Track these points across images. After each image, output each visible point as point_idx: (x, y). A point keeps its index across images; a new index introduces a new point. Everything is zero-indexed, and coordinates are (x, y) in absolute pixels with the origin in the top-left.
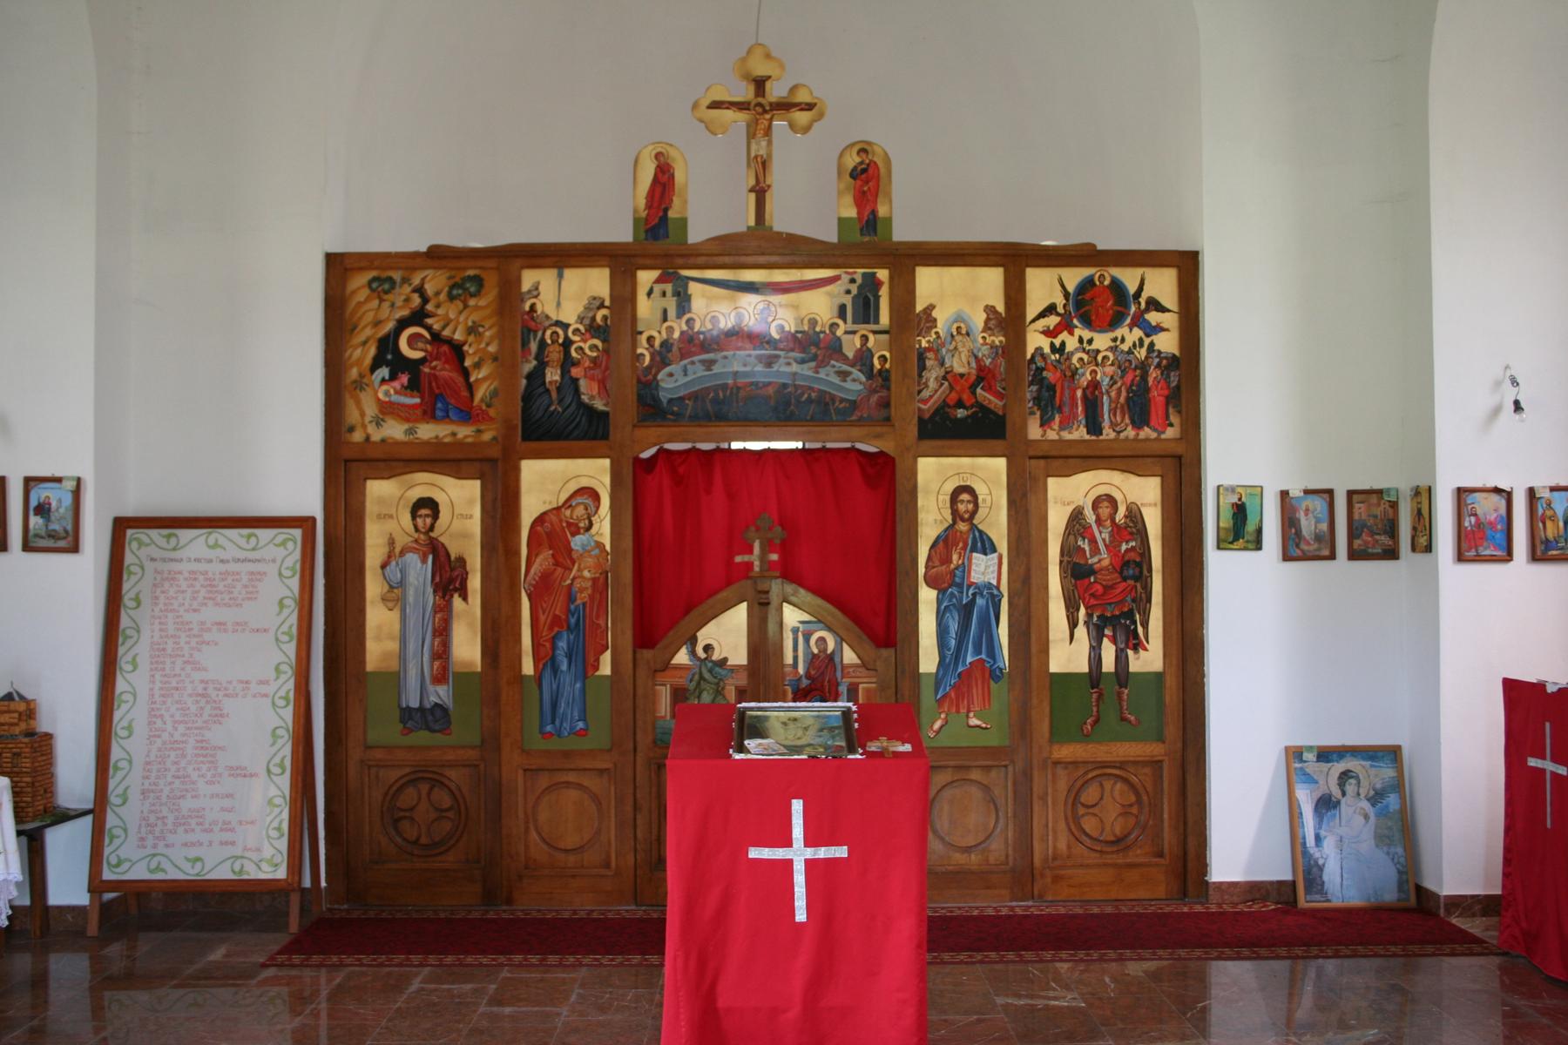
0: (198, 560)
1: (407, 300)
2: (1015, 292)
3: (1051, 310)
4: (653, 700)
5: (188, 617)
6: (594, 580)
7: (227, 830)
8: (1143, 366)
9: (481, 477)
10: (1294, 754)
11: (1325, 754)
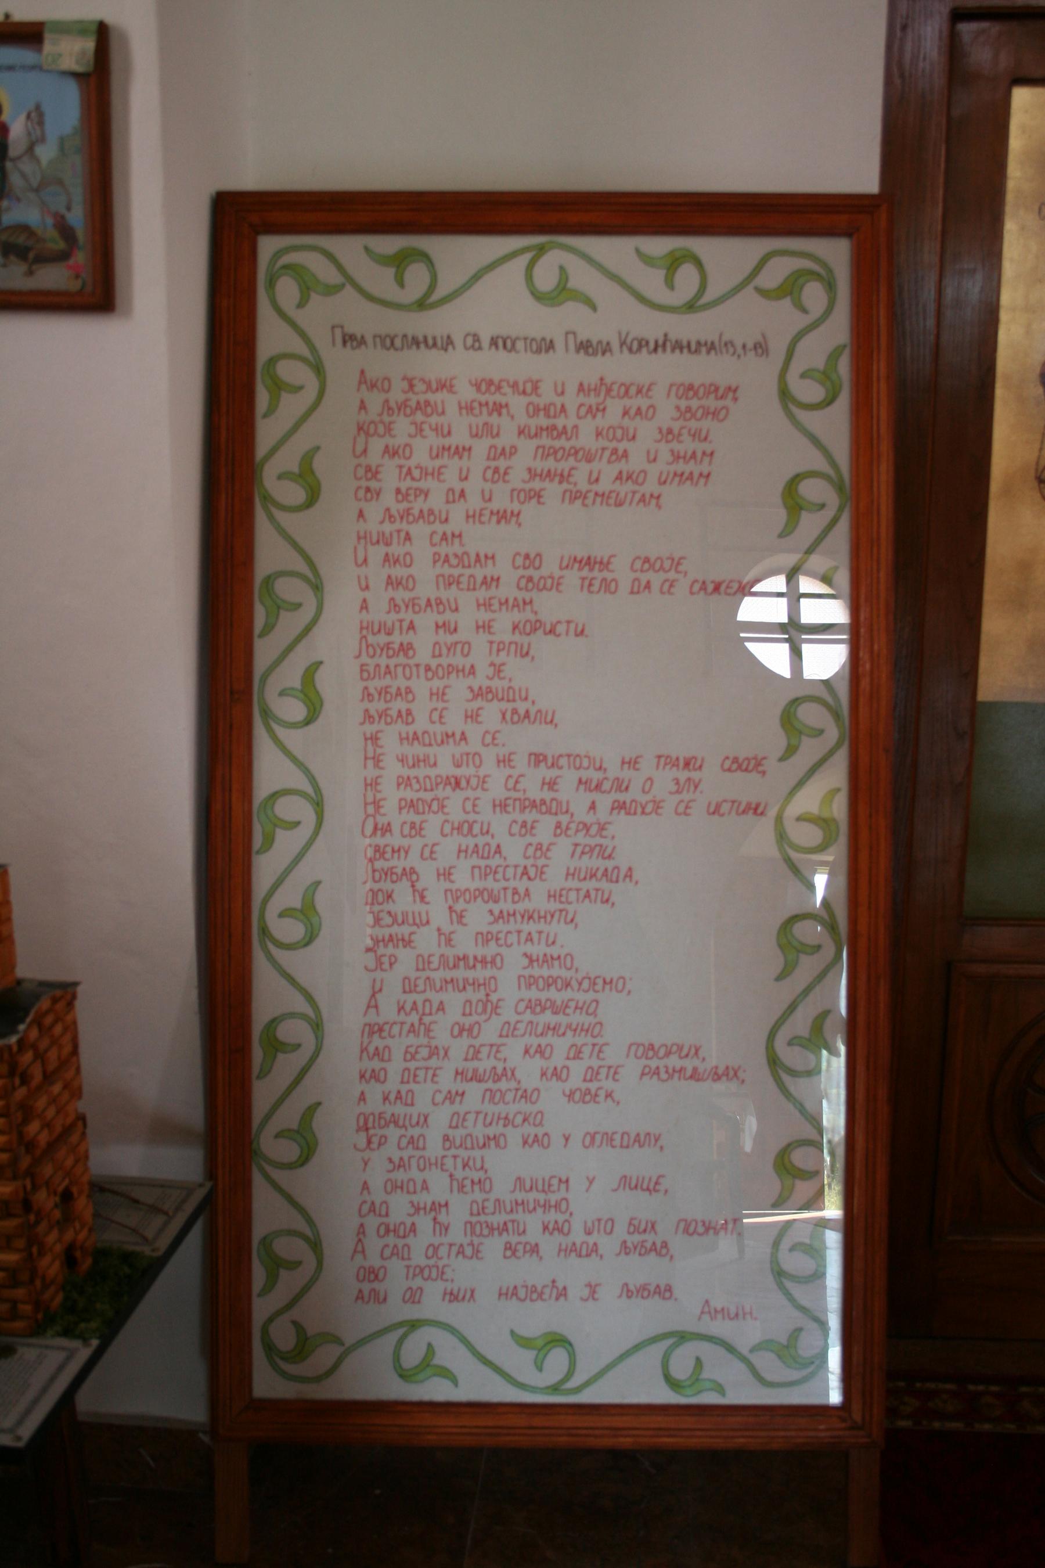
0: (502, 343)
5: (479, 538)
7: (644, 1250)
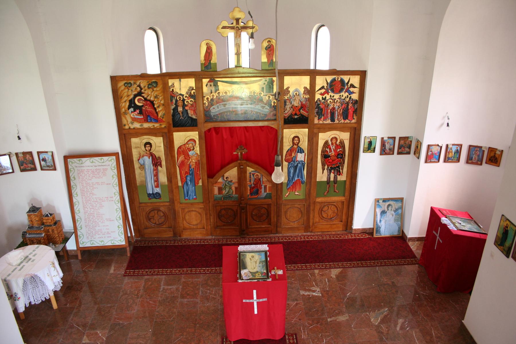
0: (88, 166)
1: (136, 89)
2: (313, 83)
3: (323, 87)
4: (212, 190)
5: (88, 182)
6: (196, 162)
8: (348, 103)
9: (163, 136)
10: (377, 201)
11: (384, 200)
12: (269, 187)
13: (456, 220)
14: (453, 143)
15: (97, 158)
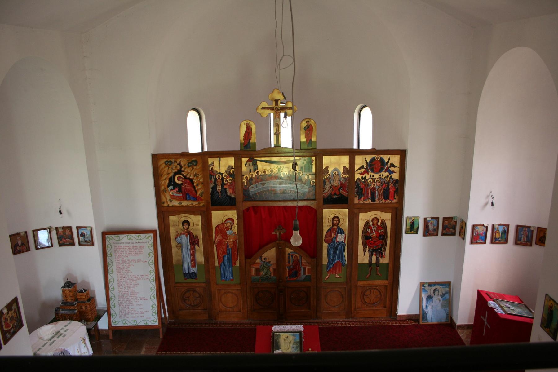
1: (176, 167)
2: (352, 163)
3: (362, 167)
5: (125, 259)
6: (233, 242)
8: (388, 183)
9: (201, 215)
10: (422, 285)
11: (430, 284)
12: (309, 269)
13: (504, 304)
14: (499, 223)
15: (134, 235)
